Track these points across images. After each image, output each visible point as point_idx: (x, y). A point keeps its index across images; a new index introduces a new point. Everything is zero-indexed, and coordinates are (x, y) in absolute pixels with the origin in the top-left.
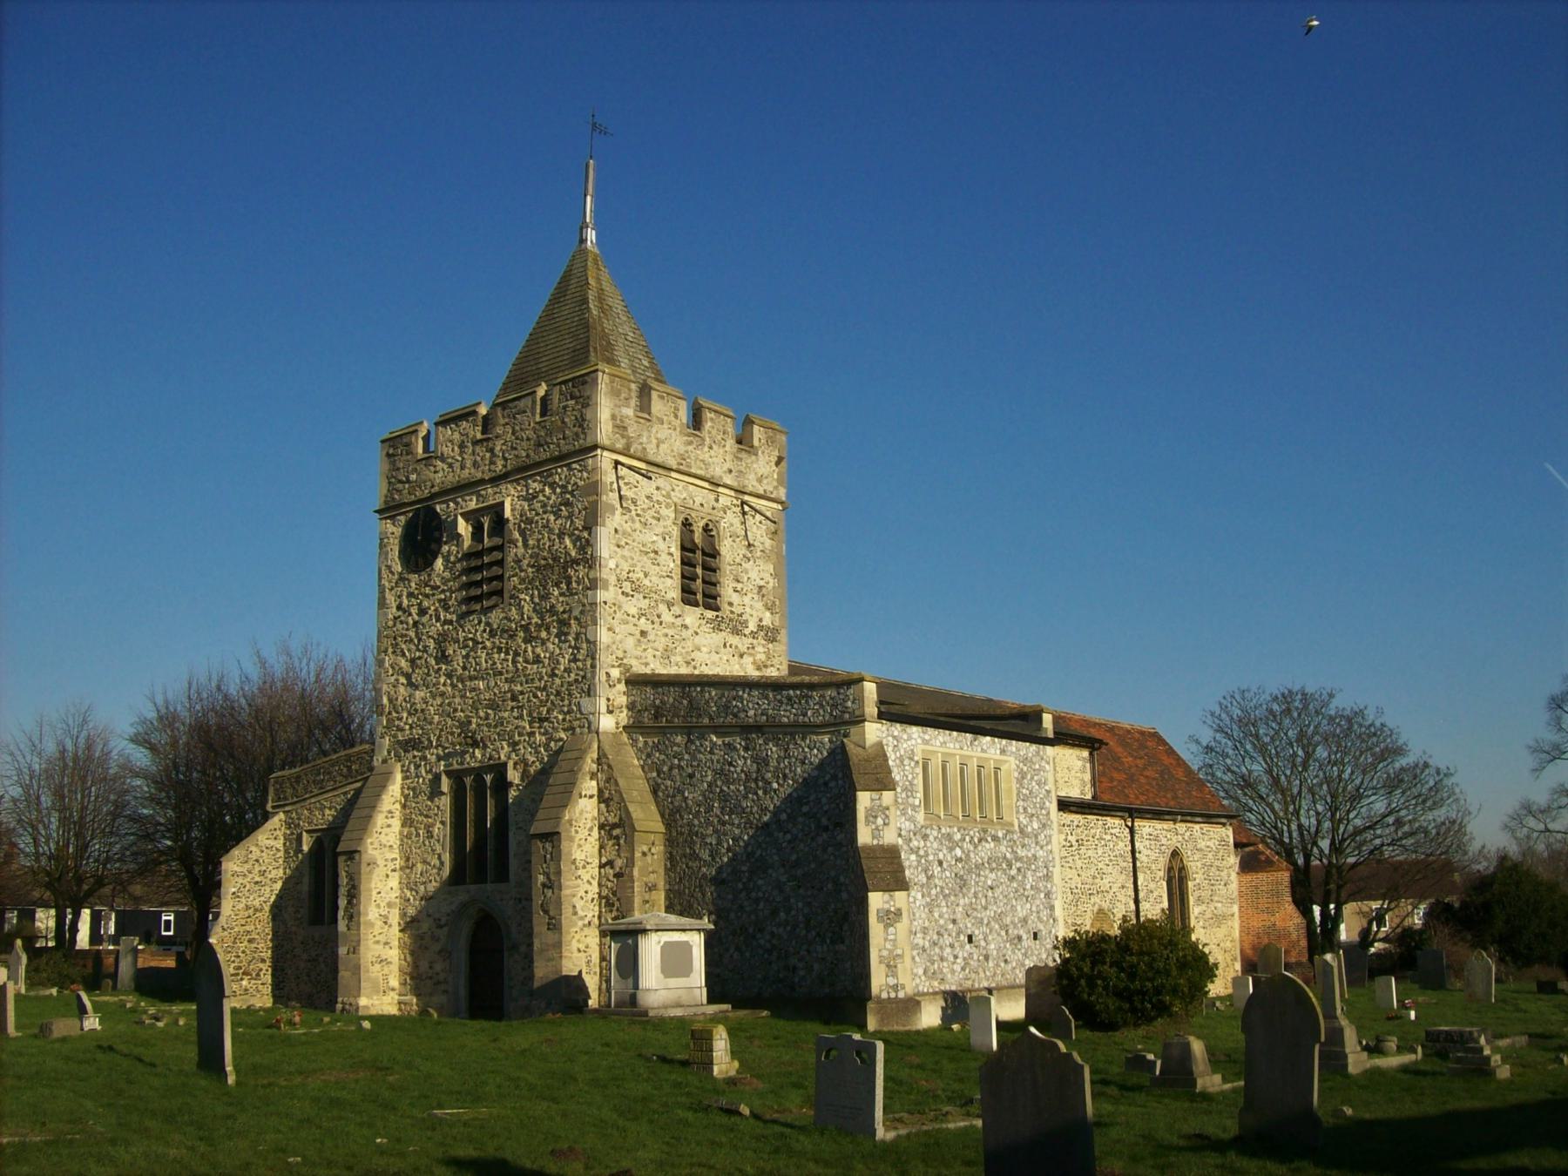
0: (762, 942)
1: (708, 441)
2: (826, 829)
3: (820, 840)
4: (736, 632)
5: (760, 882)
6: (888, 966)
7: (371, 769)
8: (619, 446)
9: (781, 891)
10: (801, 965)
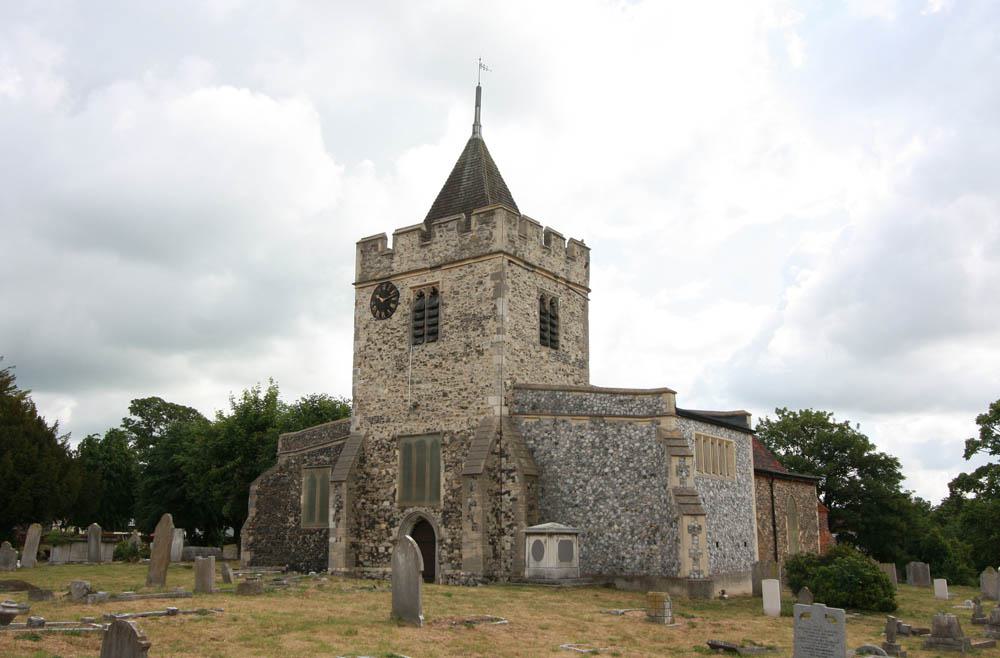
0: (603, 541)
1: (553, 253)
2: (645, 477)
3: (641, 484)
4: (565, 362)
5: (601, 507)
6: (694, 559)
7: (349, 433)
8: (512, 252)
9: (615, 512)
10: (628, 556)
